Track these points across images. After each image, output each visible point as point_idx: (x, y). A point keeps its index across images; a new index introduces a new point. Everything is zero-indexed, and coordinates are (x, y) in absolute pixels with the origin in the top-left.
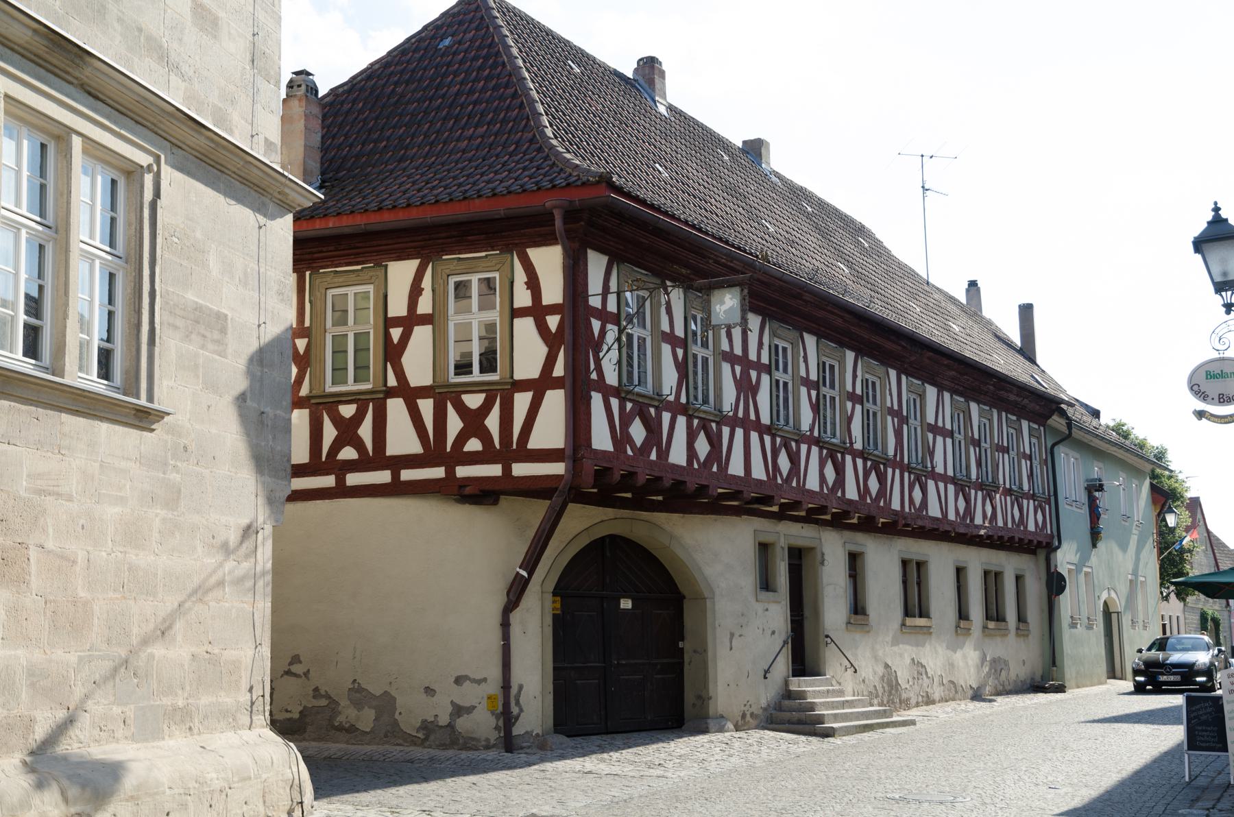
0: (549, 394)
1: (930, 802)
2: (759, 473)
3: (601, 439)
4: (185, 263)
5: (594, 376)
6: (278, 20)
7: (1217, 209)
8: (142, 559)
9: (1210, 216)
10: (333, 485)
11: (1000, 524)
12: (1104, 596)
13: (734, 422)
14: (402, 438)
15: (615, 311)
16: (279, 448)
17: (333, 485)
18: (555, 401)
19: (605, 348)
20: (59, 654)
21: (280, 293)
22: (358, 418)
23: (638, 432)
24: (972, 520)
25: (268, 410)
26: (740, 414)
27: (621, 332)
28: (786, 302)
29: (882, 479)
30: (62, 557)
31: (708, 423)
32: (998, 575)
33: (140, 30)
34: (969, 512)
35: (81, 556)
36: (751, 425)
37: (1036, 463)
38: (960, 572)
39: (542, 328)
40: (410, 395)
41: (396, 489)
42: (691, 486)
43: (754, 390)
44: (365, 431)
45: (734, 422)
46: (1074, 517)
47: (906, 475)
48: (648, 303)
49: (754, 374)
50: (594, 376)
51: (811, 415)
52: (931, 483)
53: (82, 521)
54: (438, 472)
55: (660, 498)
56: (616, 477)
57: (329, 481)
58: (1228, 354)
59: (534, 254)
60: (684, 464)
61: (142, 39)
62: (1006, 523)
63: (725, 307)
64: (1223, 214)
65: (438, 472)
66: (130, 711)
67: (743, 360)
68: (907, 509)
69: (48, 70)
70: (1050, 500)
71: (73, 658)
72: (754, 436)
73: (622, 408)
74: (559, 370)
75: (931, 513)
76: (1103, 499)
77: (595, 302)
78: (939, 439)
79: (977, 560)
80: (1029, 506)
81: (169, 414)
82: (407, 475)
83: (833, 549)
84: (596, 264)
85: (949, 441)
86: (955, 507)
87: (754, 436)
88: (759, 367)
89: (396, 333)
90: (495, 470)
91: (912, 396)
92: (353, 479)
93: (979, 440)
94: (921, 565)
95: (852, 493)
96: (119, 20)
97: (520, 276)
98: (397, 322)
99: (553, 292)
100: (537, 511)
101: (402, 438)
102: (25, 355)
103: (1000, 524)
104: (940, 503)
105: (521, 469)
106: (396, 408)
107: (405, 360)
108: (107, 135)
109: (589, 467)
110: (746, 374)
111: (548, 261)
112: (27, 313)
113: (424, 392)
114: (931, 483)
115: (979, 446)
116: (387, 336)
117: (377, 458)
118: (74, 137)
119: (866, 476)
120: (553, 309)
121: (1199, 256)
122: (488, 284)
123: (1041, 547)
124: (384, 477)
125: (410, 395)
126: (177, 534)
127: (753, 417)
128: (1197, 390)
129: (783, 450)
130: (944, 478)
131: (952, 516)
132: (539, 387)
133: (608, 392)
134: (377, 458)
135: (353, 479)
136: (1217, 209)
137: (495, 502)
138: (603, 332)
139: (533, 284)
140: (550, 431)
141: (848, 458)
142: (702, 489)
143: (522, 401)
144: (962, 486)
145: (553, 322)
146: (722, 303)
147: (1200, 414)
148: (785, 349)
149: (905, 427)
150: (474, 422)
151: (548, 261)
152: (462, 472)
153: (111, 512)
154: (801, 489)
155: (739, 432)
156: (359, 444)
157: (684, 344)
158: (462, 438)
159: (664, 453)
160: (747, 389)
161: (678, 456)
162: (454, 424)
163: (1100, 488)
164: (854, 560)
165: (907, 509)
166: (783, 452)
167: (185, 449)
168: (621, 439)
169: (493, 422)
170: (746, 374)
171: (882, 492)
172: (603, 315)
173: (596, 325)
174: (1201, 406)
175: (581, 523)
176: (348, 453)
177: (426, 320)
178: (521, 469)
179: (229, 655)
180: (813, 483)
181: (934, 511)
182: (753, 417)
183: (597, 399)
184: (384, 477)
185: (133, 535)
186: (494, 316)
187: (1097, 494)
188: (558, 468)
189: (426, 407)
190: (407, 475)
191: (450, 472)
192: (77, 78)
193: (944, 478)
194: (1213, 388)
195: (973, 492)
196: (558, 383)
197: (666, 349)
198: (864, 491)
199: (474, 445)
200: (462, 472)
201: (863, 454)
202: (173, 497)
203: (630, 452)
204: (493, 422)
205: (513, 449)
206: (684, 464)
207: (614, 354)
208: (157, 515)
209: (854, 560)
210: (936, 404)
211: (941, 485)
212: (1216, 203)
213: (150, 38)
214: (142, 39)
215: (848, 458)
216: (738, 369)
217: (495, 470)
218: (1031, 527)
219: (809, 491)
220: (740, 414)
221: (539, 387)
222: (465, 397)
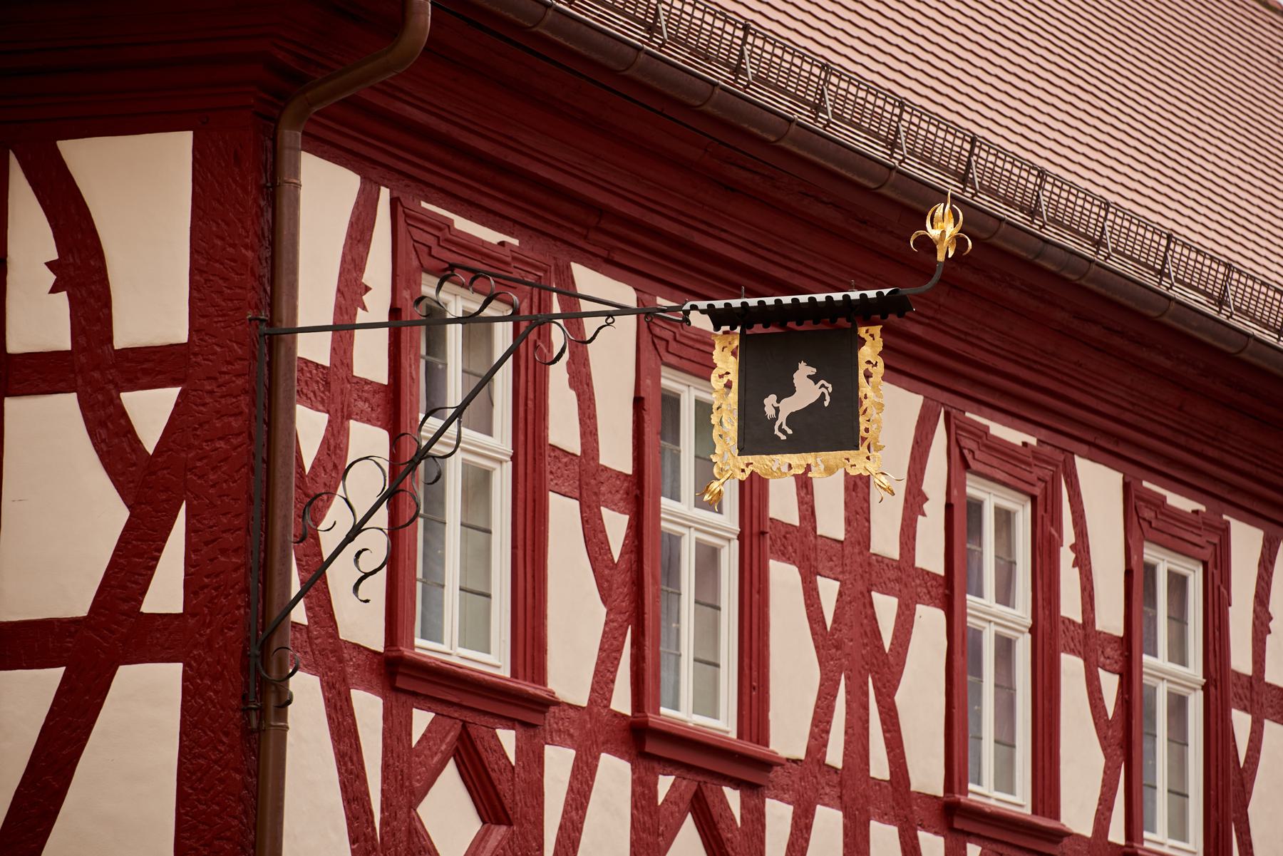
0: (129, 677)
5: (299, 614)
10: (1111, 838)
17: (1111, 838)
18: (146, 704)
26: (835, 755)
39: (110, 433)
49: (886, 607)
50: (299, 614)
51: (1099, 760)
59: (92, 161)
63: (791, 405)
73: (395, 728)
74: (165, 592)
77: (314, 349)
91: (1163, 562)
97: (32, 238)
99: (153, 305)
110: (856, 606)
120: (150, 366)
127: (879, 767)
129: (689, 825)
145: (150, 411)
146: (787, 390)
148: (1178, 583)
157: (638, 494)
160: (861, 662)
170: (856, 606)
172: (336, 389)
173: (310, 426)
182: (879, 767)
196: (152, 640)
216: (829, 589)
220: (835, 755)
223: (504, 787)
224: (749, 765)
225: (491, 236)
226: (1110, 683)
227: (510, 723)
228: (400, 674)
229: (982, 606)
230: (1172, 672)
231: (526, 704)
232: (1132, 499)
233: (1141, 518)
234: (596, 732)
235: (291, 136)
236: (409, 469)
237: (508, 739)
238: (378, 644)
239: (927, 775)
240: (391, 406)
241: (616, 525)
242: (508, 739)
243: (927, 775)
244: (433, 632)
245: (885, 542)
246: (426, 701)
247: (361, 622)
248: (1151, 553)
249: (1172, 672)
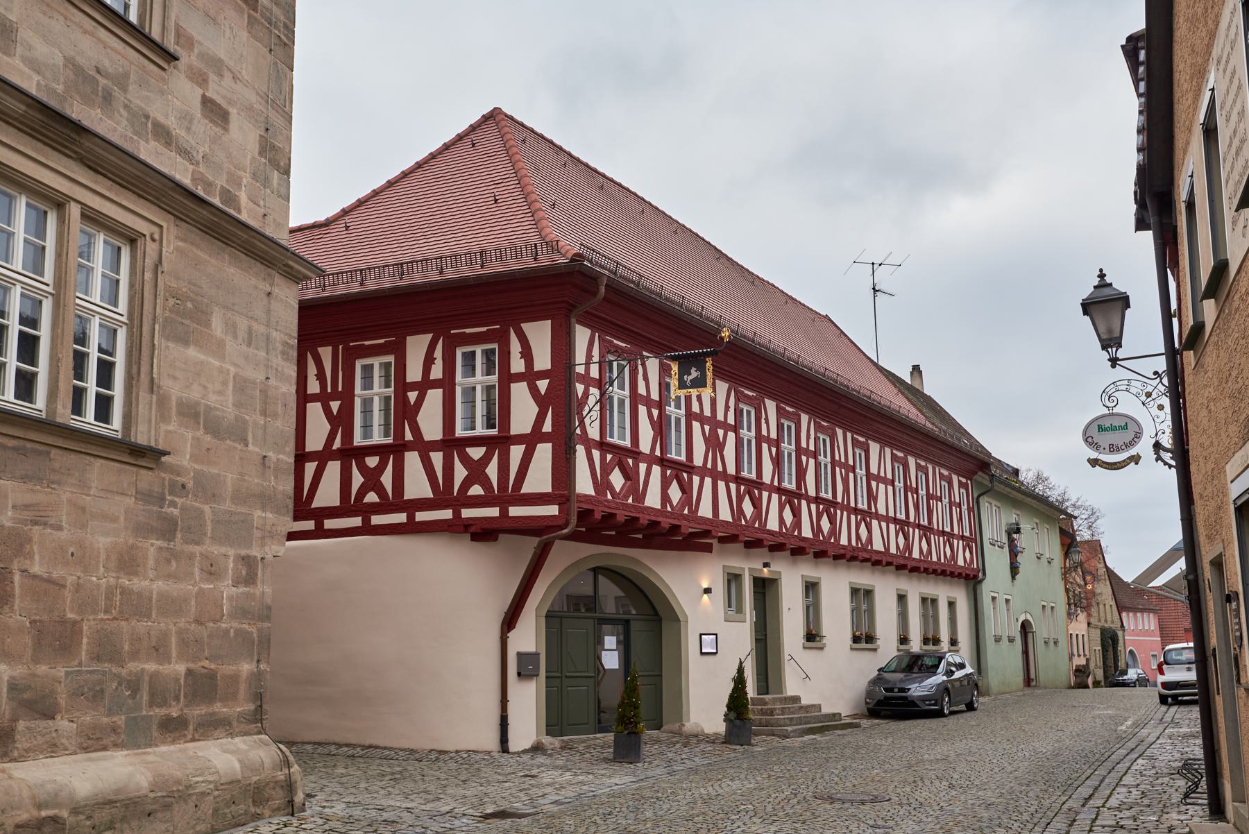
1: (852, 801)
2: (725, 515)
3: (584, 485)
4: (187, 322)
5: (578, 431)
6: (289, 119)
7: (1102, 276)
8: (137, 584)
9: (1096, 281)
11: (935, 559)
12: (1022, 618)
13: (703, 472)
14: (417, 485)
15: (597, 377)
16: (281, 488)
18: (544, 451)
19: (587, 409)
20: (43, 669)
21: (283, 353)
22: (381, 468)
23: (617, 479)
24: (910, 553)
25: (270, 454)
26: (709, 465)
27: (602, 395)
28: (757, 370)
29: (832, 520)
30: (49, 581)
31: (679, 471)
32: (934, 601)
33: (147, 117)
34: (909, 547)
35: (71, 579)
36: (716, 476)
37: (964, 507)
38: (902, 598)
39: (534, 390)
40: (424, 448)
41: (411, 528)
42: (621, 516)
43: (721, 446)
44: (387, 479)
45: (703, 472)
46: (996, 561)
47: (853, 517)
48: (627, 370)
49: (721, 432)
50: (578, 431)
52: (875, 523)
53: (71, 550)
54: (447, 514)
55: (640, 536)
56: (598, 516)
57: (356, 521)
58: (1116, 410)
60: (659, 507)
61: (150, 125)
62: (939, 559)
64: (1108, 279)
65: (447, 514)
66: (120, 720)
67: (712, 421)
68: (854, 543)
69: (45, 144)
70: (974, 541)
71: (60, 672)
72: (721, 484)
74: (547, 427)
75: (875, 548)
76: (1022, 541)
77: (580, 369)
78: (882, 486)
79: (916, 589)
80: (959, 544)
81: (169, 453)
82: (421, 516)
83: (791, 580)
84: (582, 335)
85: (890, 488)
86: (896, 543)
87: (721, 484)
88: (725, 426)
89: (412, 396)
90: (494, 512)
91: (858, 451)
92: (377, 520)
93: (917, 488)
94: (869, 593)
95: (807, 532)
96: (126, 107)
98: (414, 386)
99: (543, 361)
100: (531, 544)
101: (417, 485)
102: (16, 397)
103: (935, 559)
104: (880, 538)
105: (514, 511)
106: (412, 459)
107: (420, 419)
108: (108, 204)
109: (574, 509)
110: (714, 432)
111: (540, 334)
112: (20, 358)
113: (434, 445)
114: (875, 523)
115: (917, 493)
116: (406, 399)
117: (397, 502)
118: (73, 204)
119: (740, 499)
120: (543, 375)
121: (1087, 318)
122: (488, 354)
123: (972, 579)
124: (401, 518)
125: (424, 448)
126: (174, 563)
127: (720, 468)
128: (1089, 440)
130: (887, 519)
131: (893, 550)
132: (531, 440)
133: (589, 444)
134: (397, 502)
135: (377, 520)
136: (1102, 276)
137: (496, 539)
138: (586, 394)
139: (527, 354)
140: (539, 478)
141: (804, 503)
142: (675, 529)
143: (517, 452)
144: (902, 525)
145: (543, 385)
147: (1094, 462)
148: (789, 427)
149: (851, 475)
150: (476, 472)
151: (540, 334)
152: (467, 513)
153: (102, 542)
154: (910, 558)
155: (708, 481)
156: (381, 491)
157: (661, 405)
158: (466, 484)
159: (640, 497)
160: (715, 445)
161: (653, 499)
162: (460, 473)
163: (1018, 531)
164: (811, 588)
165: (854, 543)
166: (675, 484)
167: (183, 486)
168: (602, 485)
169: (492, 471)
170: (714, 432)
171: (833, 531)
172: (586, 379)
173: (580, 388)
174: (1094, 455)
175: (567, 556)
176: (372, 497)
177: (435, 384)
178: (514, 511)
179: (228, 669)
180: (773, 524)
181: (878, 545)
182: (720, 468)
183: (580, 450)
184: (401, 518)
185: (128, 563)
186: (494, 379)
187: (1015, 536)
188: (553, 510)
189: (437, 458)
190: (421, 516)
191: (457, 514)
192: (76, 152)
193: (887, 519)
194: (1105, 439)
195: (839, 512)
197: (696, 425)
198: (817, 530)
199: (476, 490)
200: (467, 513)
201: (818, 500)
202: (168, 529)
203: (609, 497)
204: (492, 471)
205: (509, 495)
206: (659, 507)
207: (595, 413)
208: (152, 547)
209: (811, 588)
210: (879, 457)
211: (884, 524)
212: (1101, 270)
213: (157, 126)
214: (150, 125)
215: (804, 503)
216: (707, 428)
217: (494, 512)
218: (961, 562)
219: (770, 532)
220: (709, 465)
221: (531, 440)
222: (469, 450)
224: (689, 468)
226: (774, 450)
228: (603, 446)
229: (858, 470)
230: (922, 492)
231: (635, 453)
232: (778, 409)
233: (918, 467)
234: (651, 460)
235: (573, 320)
236: (817, 465)
237: (630, 461)
238: (598, 439)
239: (731, 470)
240: (600, 384)
241: (655, 413)
242: (630, 461)
243: (731, 470)
244: (612, 437)
245: (720, 417)
246: (670, 468)
247: (812, 492)
248: (741, 405)
249: (922, 492)
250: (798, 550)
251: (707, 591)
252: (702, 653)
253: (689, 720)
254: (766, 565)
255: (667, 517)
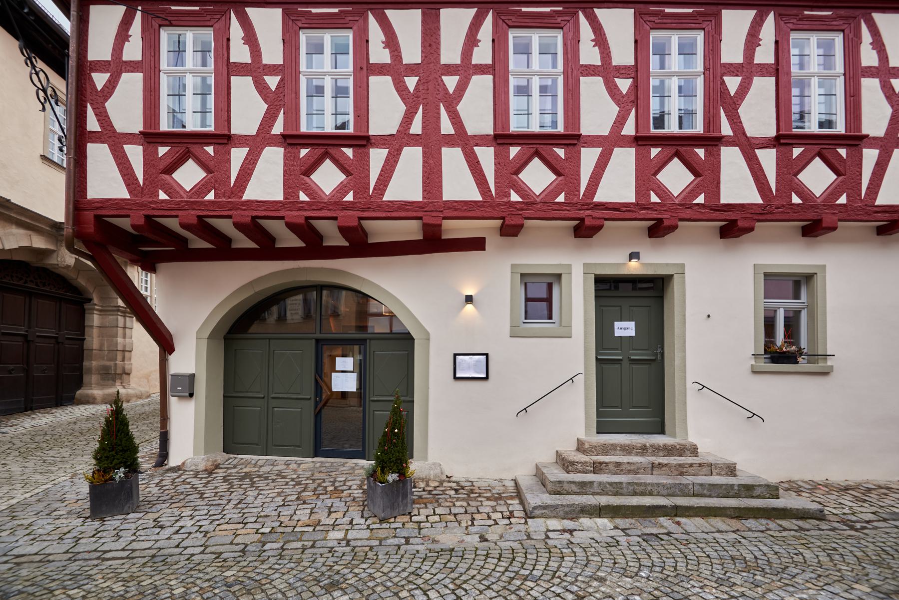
43: (452, 101)
223: (211, 164)
225: (547, 10)
227: (209, 144)
237: (843, 152)
242: (843, 152)
246: (304, 146)
250: (733, 225)
251: (469, 299)
252: (455, 378)
253: (425, 458)
254: (634, 256)
255: (298, 210)
